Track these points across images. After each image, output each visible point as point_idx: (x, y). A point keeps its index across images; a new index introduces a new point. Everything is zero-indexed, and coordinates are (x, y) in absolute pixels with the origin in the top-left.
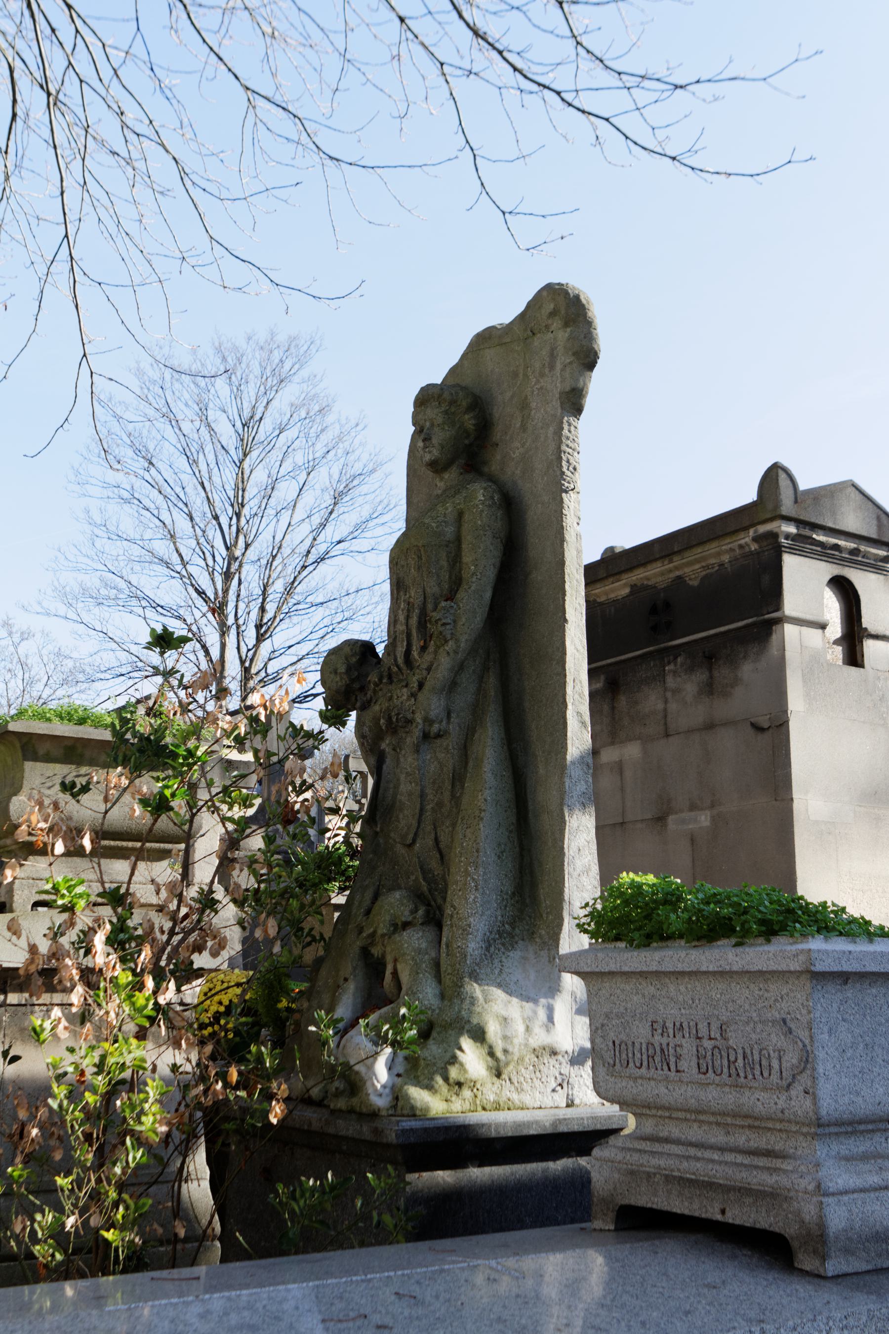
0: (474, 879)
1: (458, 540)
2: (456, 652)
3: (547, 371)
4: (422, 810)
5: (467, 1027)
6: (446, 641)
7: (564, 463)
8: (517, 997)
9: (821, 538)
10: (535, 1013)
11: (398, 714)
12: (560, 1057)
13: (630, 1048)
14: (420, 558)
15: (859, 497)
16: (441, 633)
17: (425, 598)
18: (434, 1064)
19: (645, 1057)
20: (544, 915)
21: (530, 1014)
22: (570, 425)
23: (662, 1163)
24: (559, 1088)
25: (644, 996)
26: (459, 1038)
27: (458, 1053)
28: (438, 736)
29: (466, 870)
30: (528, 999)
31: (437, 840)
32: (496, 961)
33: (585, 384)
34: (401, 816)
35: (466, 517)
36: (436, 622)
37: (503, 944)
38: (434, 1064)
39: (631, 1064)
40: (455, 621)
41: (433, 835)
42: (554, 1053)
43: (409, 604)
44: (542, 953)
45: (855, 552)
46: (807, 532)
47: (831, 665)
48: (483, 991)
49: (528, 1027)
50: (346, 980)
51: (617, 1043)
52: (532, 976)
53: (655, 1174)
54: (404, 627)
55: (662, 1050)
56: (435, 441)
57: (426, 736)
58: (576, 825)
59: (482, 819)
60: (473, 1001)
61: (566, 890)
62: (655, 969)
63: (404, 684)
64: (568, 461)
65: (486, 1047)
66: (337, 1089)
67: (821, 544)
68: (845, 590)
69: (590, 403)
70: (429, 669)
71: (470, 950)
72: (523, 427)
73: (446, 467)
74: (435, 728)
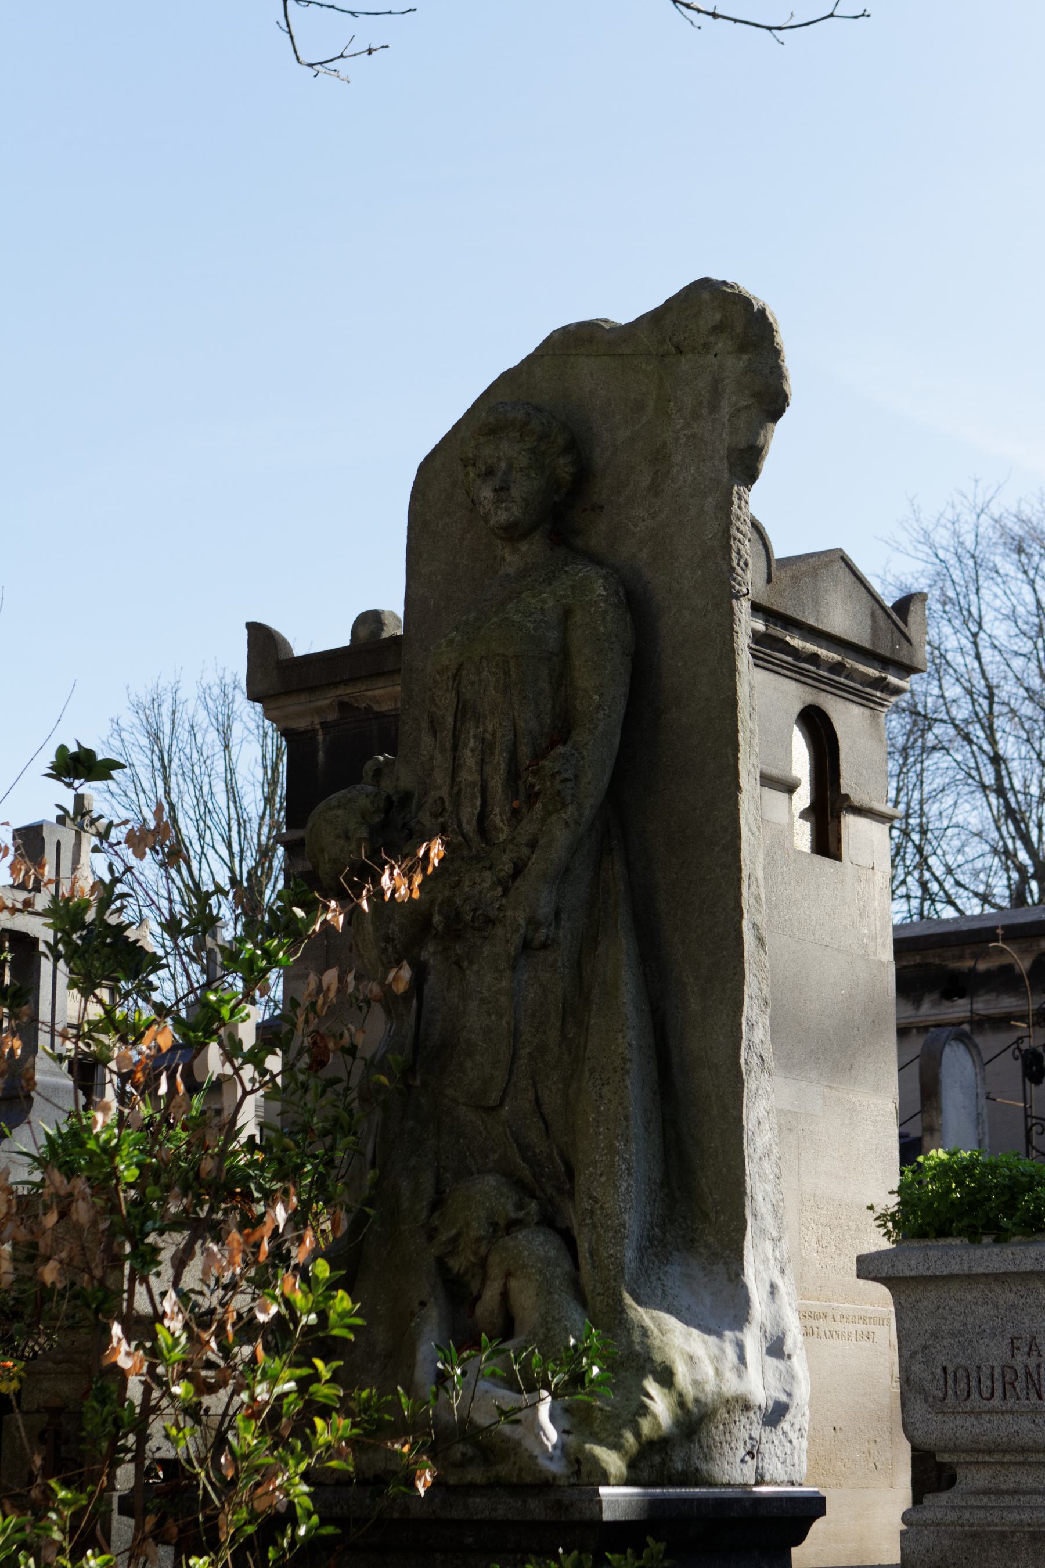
0: (624, 1159)
1: (564, 653)
2: (577, 823)
3: (705, 412)
4: (514, 1057)
5: (648, 1366)
6: (564, 805)
7: (734, 554)
8: (695, 1327)
9: (796, 642)
10: (722, 1350)
11: (475, 910)
12: (751, 1414)
13: (974, 1375)
14: (507, 673)
15: (849, 578)
16: (559, 793)
17: (515, 736)
18: (618, 1416)
19: (998, 1385)
20: (712, 1215)
21: (717, 1352)
22: (740, 498)
23: (1025, 1517)
24: (748, 1458)
25: (996, 1306)
26: (641, 1380)
27: (647, 1401)
28: (544, 946)
29: (611, 1146)
30: (707, 1330)
31: (538, 1102)
32: (653, 1278)
33: (766, 441)
34: (469, 1064)
35: (578, 617)
36: (553, 776)
37: (656, 1255)
38: (618, 1416)
39: (975, 1395)
40: (576, 777)
41: (531, 1095)
42: (747, 1407)
43: (483, 740)
44: (715, 1268)
45: (837, 668)
46: (778, 632)
47: (800, 852)
48: (652, 1318)
49: (717, 1369)
50: (423, 1304)
51: (950, 1369)
52: (708, 1300)
53: (1013, 1533)
54: (476, 777)
55: (1028, 1374)
56: (515, 492)
57: (527, 946)
58: (754, 1087)
59: (628, 1072)
60: (645, 1332)
61: (748, 1179)
62: (1029, 1268)
63: (488, 864)
64: (738, 553)
65: (675, 1394)
66: (463, 1454)
67: (794, 652)
68: (817, 726)
69: (769, 467)
70: (533, 845)
71: (627, 1260)
72: (655, 489)
73: (526, 535)
74: (542, 934)
